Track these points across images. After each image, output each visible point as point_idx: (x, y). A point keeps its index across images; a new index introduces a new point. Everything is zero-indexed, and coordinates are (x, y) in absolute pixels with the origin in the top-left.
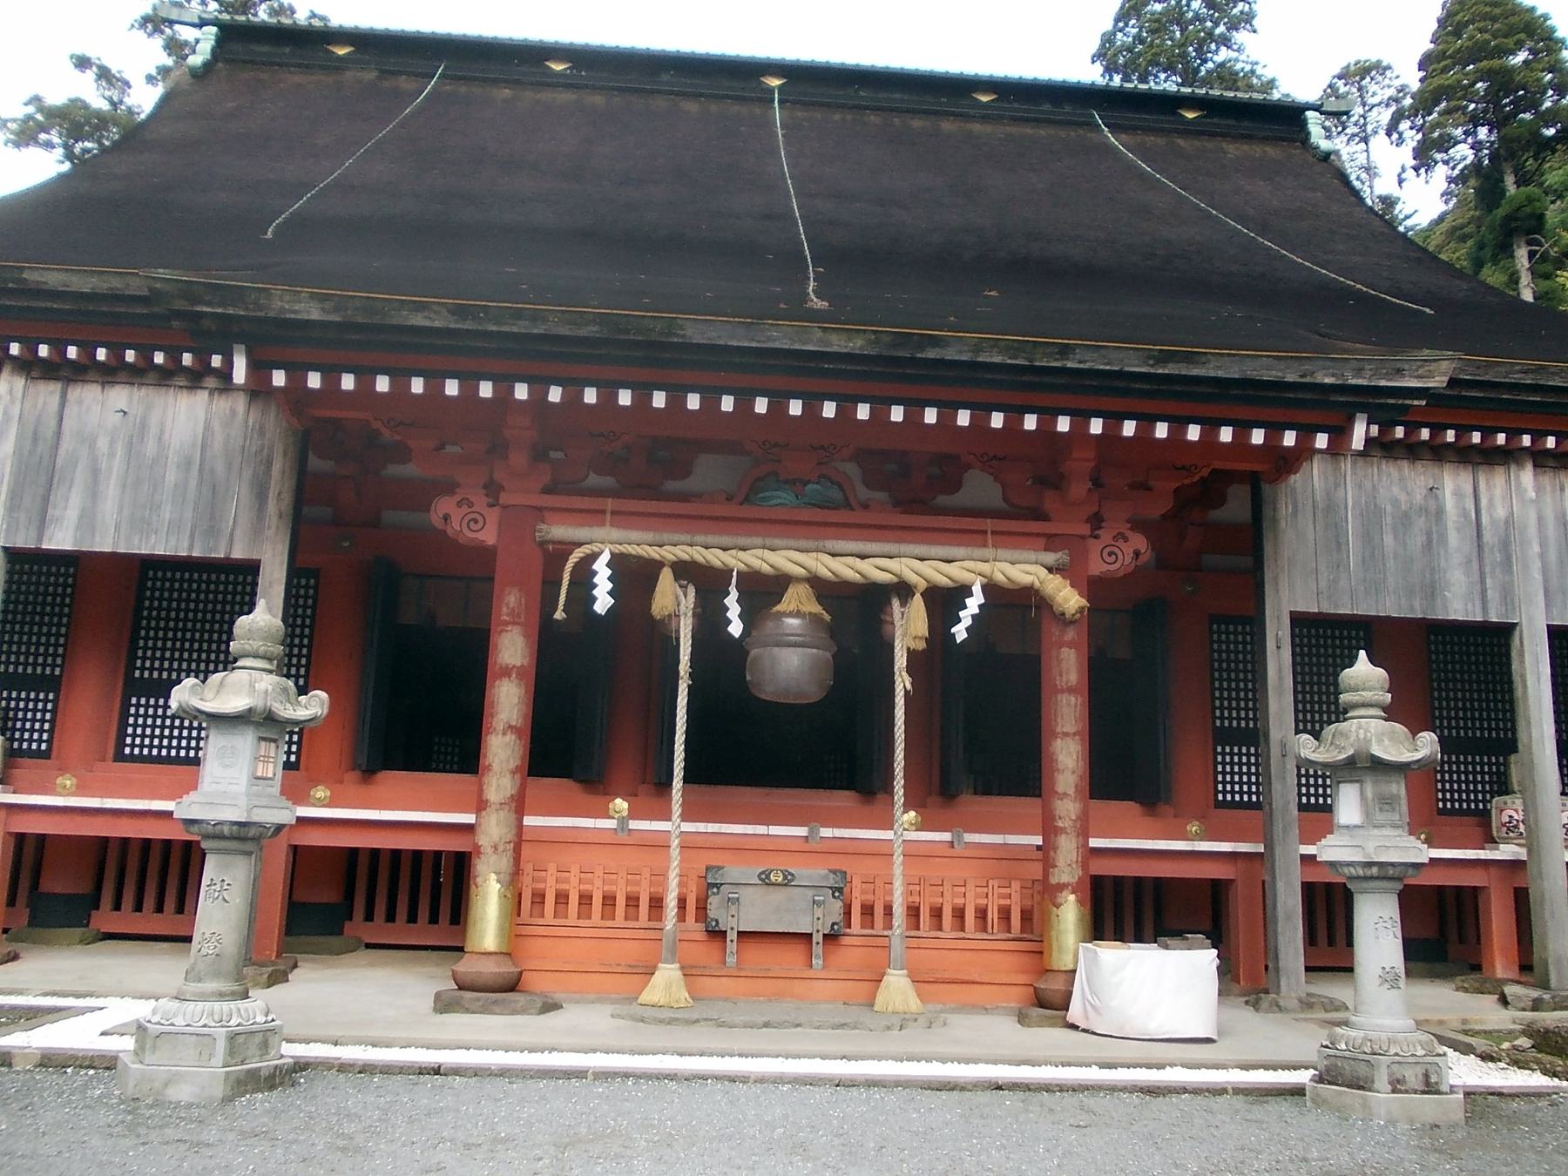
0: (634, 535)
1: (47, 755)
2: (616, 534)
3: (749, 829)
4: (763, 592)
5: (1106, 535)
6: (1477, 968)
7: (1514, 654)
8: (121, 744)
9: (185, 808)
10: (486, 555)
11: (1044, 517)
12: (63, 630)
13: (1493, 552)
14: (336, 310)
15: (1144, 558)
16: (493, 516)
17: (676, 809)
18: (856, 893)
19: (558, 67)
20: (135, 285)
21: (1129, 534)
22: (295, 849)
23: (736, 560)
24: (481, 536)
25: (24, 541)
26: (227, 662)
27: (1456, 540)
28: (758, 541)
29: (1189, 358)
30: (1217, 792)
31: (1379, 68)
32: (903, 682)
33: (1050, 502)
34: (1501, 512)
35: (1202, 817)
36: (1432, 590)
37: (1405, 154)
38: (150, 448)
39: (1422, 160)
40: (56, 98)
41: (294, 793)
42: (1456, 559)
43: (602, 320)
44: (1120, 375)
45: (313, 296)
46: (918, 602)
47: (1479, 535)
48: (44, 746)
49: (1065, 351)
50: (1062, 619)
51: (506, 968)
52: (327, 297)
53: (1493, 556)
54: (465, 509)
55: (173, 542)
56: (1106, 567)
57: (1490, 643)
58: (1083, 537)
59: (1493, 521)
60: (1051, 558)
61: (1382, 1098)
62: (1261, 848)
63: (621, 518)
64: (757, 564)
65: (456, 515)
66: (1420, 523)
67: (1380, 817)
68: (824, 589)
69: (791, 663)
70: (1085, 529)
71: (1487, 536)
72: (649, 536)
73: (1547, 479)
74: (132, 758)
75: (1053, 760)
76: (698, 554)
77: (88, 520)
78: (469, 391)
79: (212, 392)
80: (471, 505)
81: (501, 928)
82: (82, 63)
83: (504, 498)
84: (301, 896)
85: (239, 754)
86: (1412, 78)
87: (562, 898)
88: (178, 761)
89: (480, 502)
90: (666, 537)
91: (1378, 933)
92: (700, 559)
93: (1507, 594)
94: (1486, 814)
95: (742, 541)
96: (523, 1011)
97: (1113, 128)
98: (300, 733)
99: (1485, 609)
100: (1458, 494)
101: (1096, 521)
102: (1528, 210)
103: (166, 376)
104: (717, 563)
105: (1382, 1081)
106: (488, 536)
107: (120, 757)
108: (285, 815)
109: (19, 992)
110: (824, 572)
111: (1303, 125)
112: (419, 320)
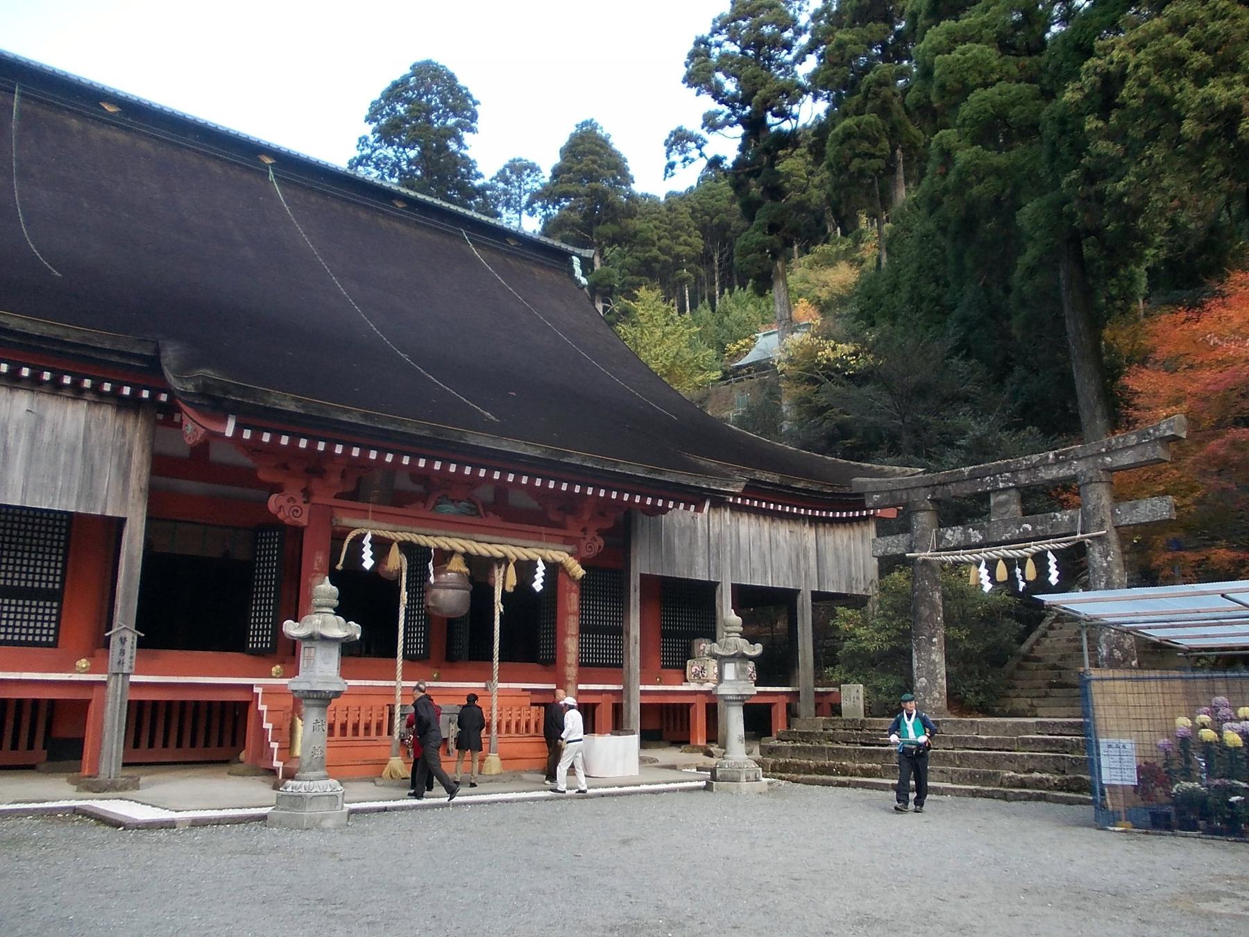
0: (384, 526)
1: (54, 645)
2: (374, 524)
3: (363, 683)
5: (588, 538)
6: (688, 742)
7: (799, 616)
10: (298, 531)
12: (59, 565)
13: (714, 549)
14: (303, 407)
16: (306, 508)
19: (111, 109)
20: (73, 337)
23: (431, 542)
24: (299, 520)
27: (701, 542)
28: (443, 532)
29: (660, 473)
31: (534, 169)
32: (499, 608)
33: (570, 520)
34: (717, 530)
38: (46, 436)
42: (701, 552)
43: (432, 429)
45: (293, 399)
46: (511, 567)
48: (51, 639)
49: (616, 464)
50: (572, 578)
52: (300, 400)
53: (713, 551)
54: (291, 504)
55: (64, 501)
57: (707, 590)
60: (569, 548)
61: (744, 785)
62: (621, 687)
63: (378, 516)
64: (442, 545)
66: (688, 533)
68: (468, 558)
70: (580, 534)
72: (391, 527)
75: (565, 647)
76: (415, 538)
78: (347, 452)
79: (89, 402)
80: (295, 501)
83: (315, 500)
86: (546, 175)
87: (367, 728)
89: (300, 499)
90: (400, 527)
91: (735, 722)
92: (414, 540)
95: (436, 532)
97: (476, 244)
102: (607, 281)
103: (56, 387)
104: (423, 543)
105: (743, 778)
106: (303, 521)
109: (44, 801)
110: (473, 551)
112: (344, 418)
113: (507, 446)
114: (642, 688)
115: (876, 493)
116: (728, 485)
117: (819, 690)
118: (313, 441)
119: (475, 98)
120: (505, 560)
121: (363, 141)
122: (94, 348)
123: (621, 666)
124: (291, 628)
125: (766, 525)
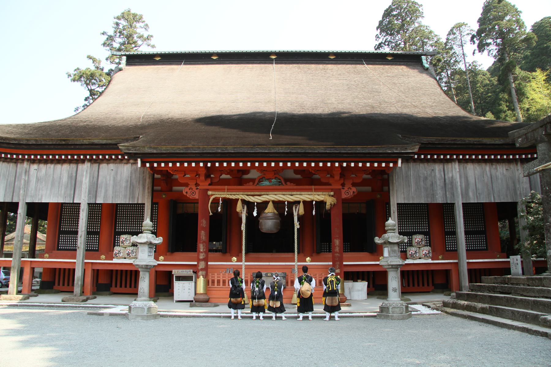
4: (263, 206)
5: (346, 188)
8: (58, 246)
9: (137, 262)
11: (330, 185)
15: (355, 193)
17: (296, 266)
18: (289, 278)
21: (352, 188)
22: (156, 271)
24: (195, 196)
25: (92, 201)
26: (385, 232)
30: (446, 248)
32: (297, 225)
34: (450, 175)
35: (311, 256)
36: (433, 195)
37: (475, 47)
39: (481, 47)
40: (83, 68)
41: (157, 258)
42: (439, 188)
44: (340, 153)
47: (445, 181)
51: (206, 297)
56: (346, 196)
57: (447, 209)
58: (340, 189)
59: (449, 178)
65: (189, 192)
67: (392, 255)
69: (269, 223)
70: (341, 187)
71: (447, 181)
73: (462, 165)
74: (61, 250)
77: (105, 196)
81: (204, 288)
82: (90, 57)
84: (158, 283)
85: (140, 250)
86: (476, 27)
87: (219, 281)
88: (71, 250)
89: (194, 188)
93: (453, 194)
94: (406, 252)
96: (210, 307)
98: (156, 245)
99: (446, 200)
100: (440, 171)
101: (343, 185)
107: (58, 249)
108: (156, 263)
109: (351, 313)
111: (421, 61)
113: (359, 149)
114: (467, 261)
115: (519, 137)
116: (406, 149)
117: (543, 259)
118: (372, 163)
119: (420, 4)
120: (298, 202)
121: (377, 37)
122: (82, 145)
123: (456, 251)
124: (377, 240)
125: (487, 168)
